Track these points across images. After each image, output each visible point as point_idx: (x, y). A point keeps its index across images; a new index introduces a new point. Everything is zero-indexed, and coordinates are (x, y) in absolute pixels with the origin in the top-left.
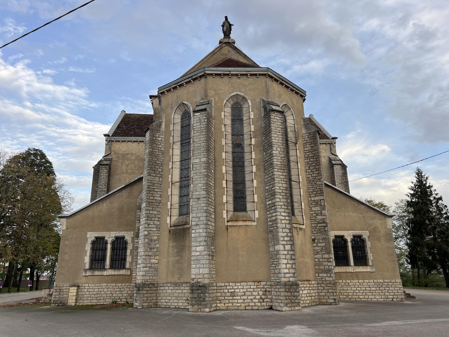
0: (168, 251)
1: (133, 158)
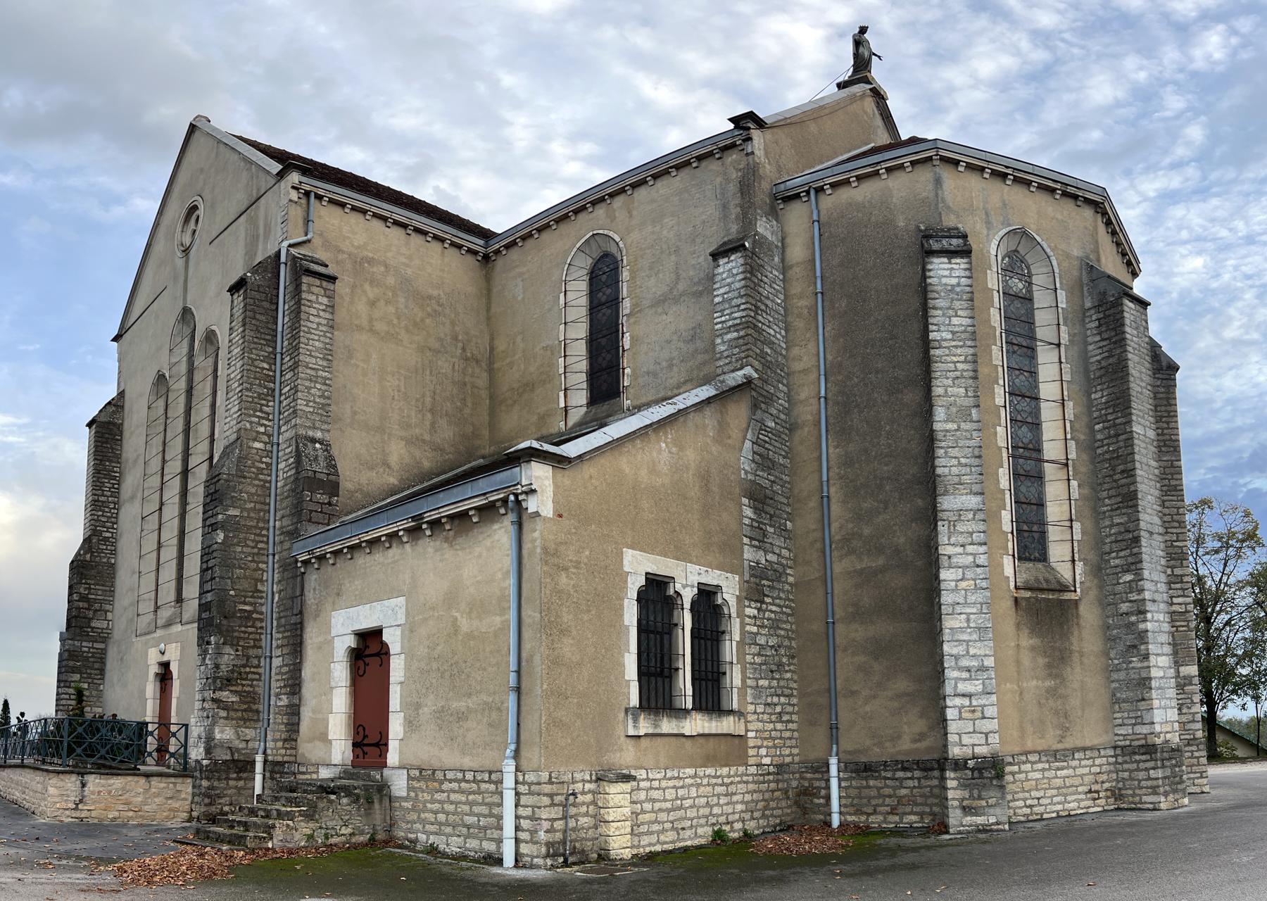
0: (1018, 662)
1: (391, 280)
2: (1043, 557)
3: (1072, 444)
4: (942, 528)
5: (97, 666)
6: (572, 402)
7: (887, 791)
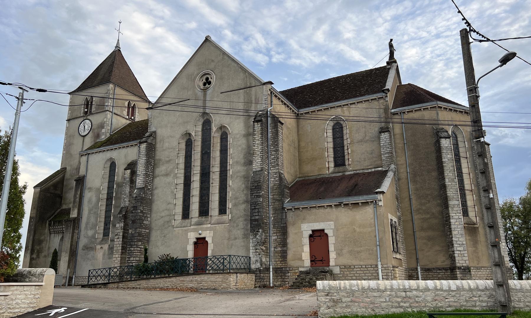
2: (468, 216)
3: (473, 185)
4: (450, 209)
5: (146, 239)
6: (330, 166)
7: (435, 276)
